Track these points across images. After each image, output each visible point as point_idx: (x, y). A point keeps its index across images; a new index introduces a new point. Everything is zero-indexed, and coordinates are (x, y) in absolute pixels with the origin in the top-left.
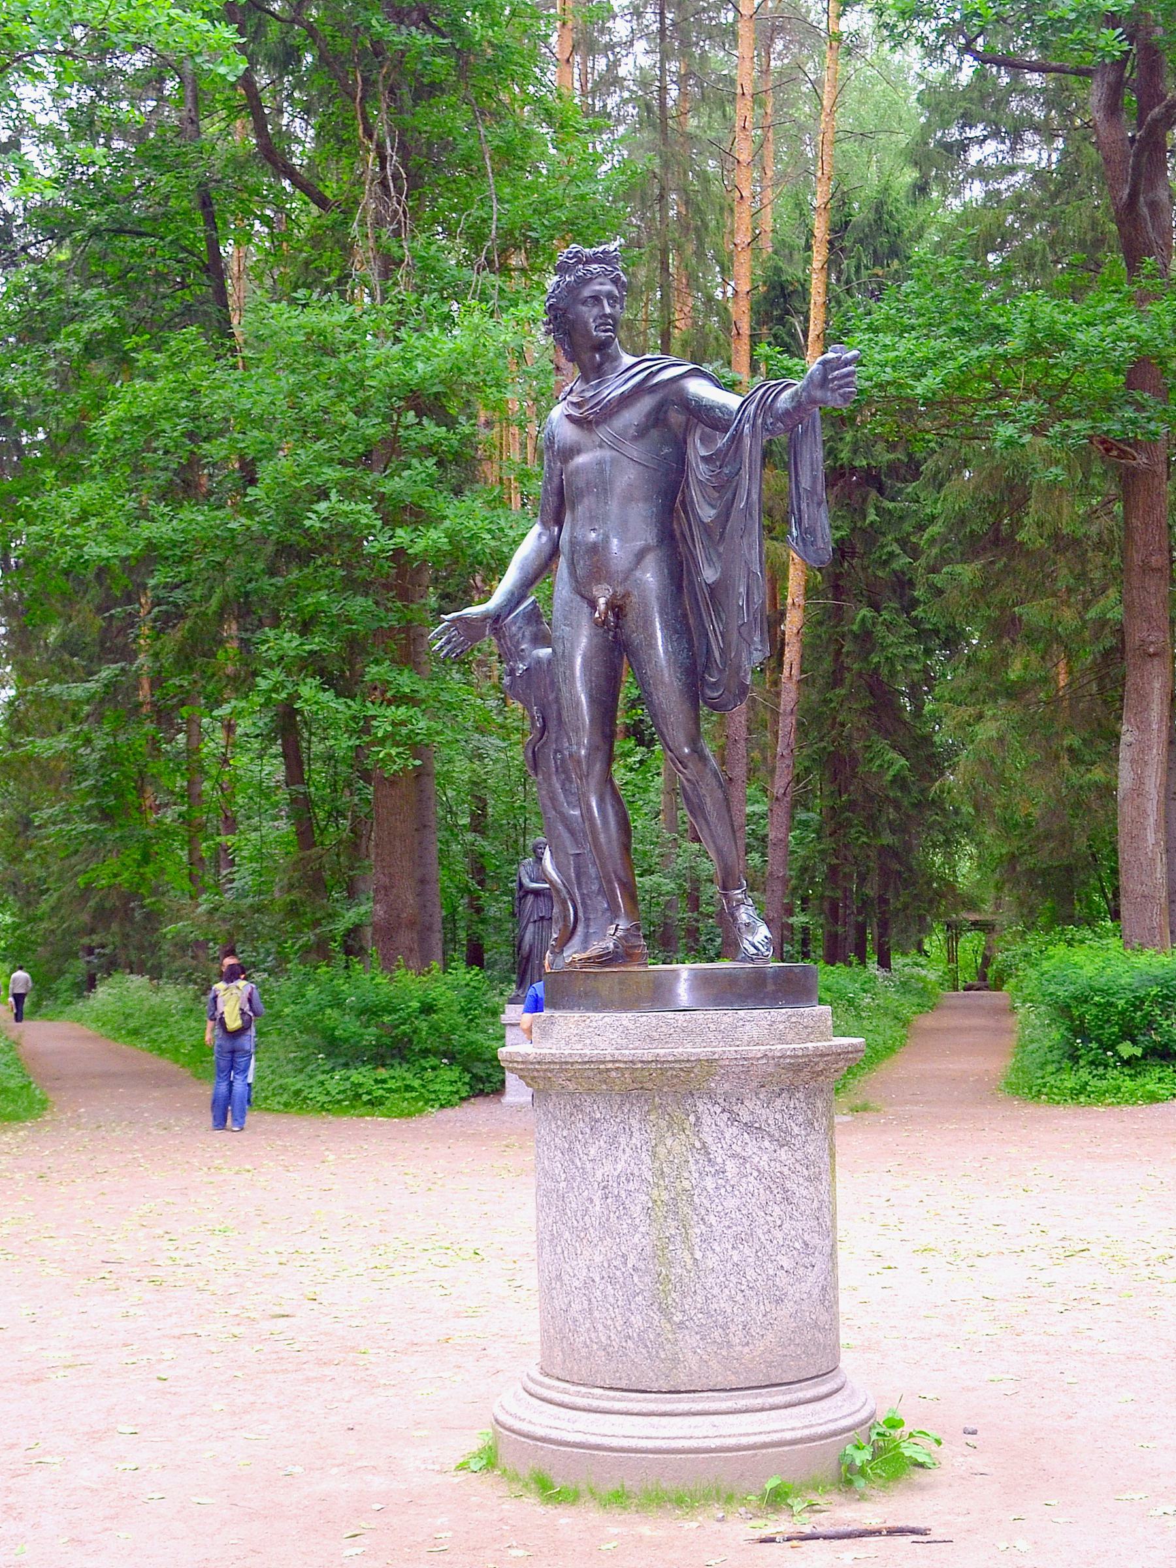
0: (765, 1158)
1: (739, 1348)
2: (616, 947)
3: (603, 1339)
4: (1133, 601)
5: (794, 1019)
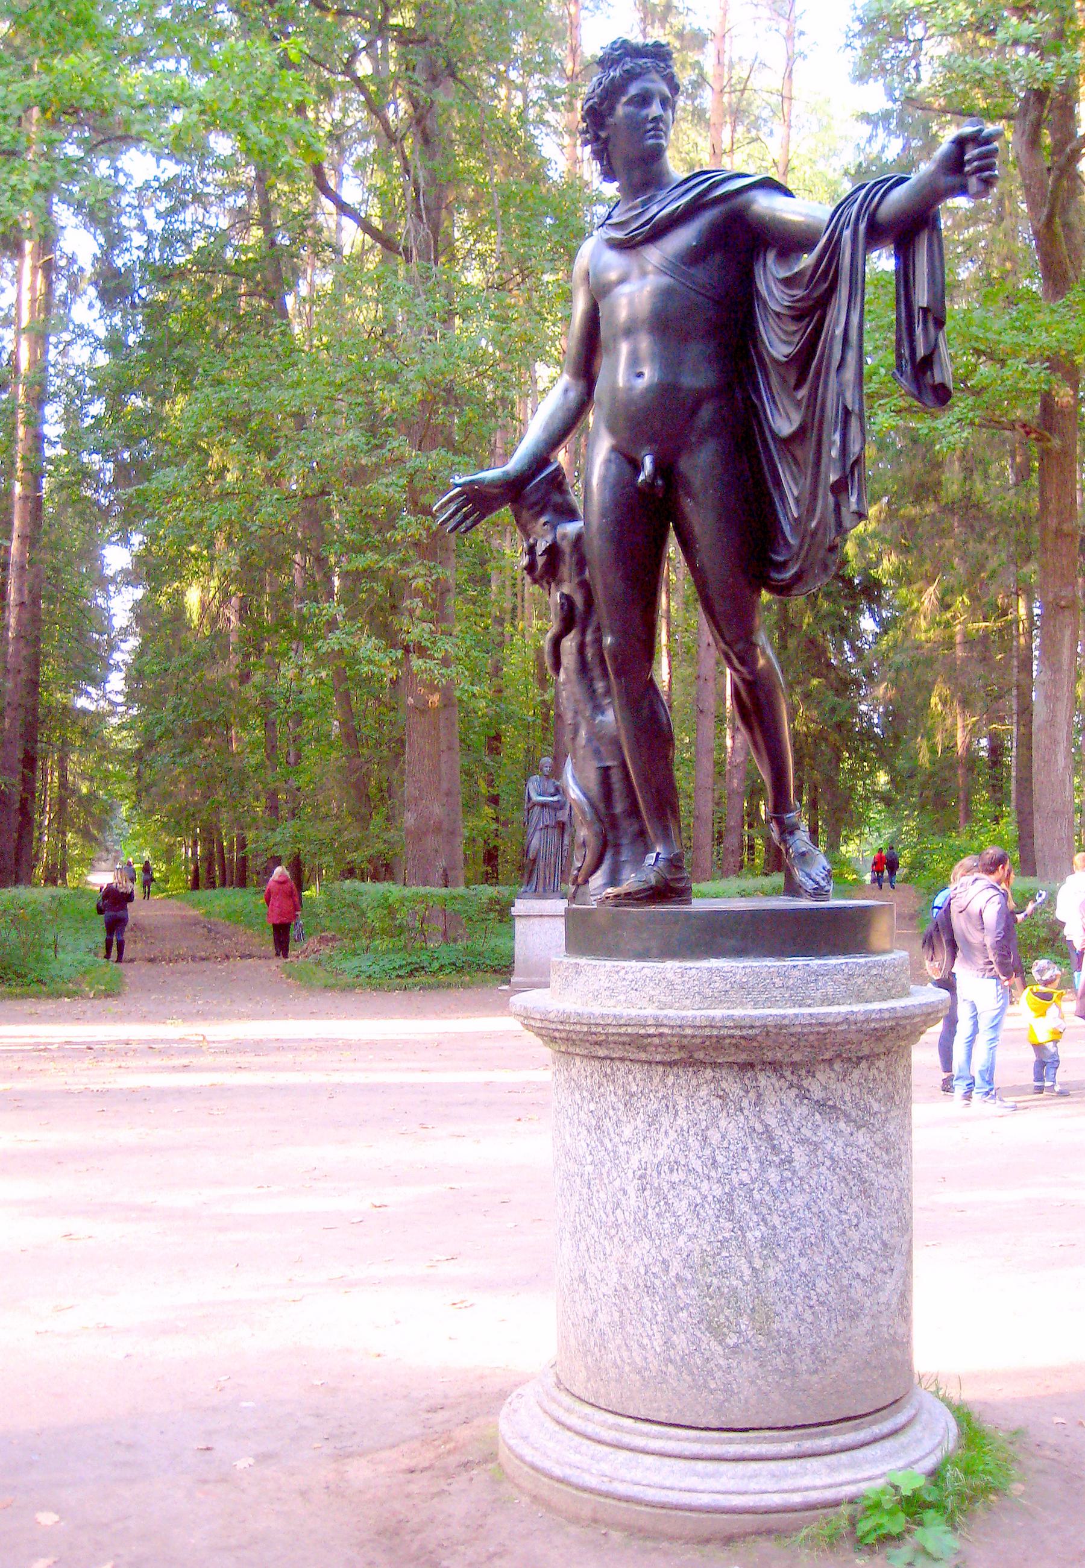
0: (840, 1142)
1: (805, 1376)
3: (638, 1360)
5: (874, 972)
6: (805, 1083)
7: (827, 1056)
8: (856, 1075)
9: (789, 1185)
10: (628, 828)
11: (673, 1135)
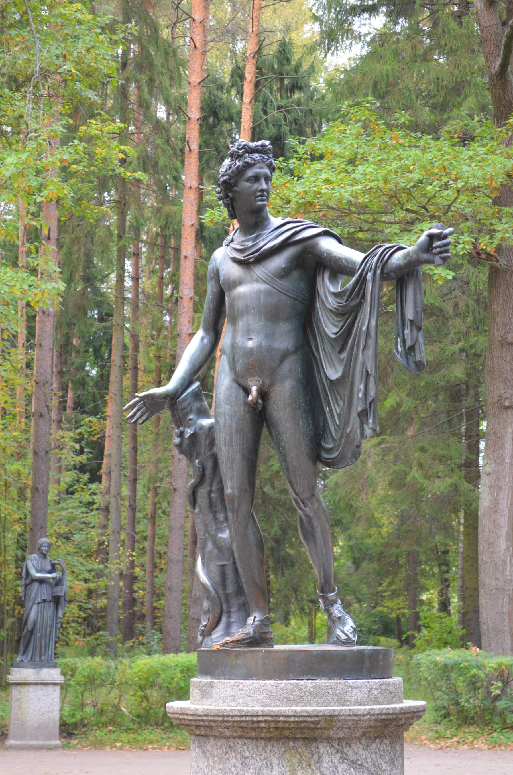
2: (255, 632)
4: (493, 367)
6: (345, 750)
8: (374, 746)
10: (235, 603)
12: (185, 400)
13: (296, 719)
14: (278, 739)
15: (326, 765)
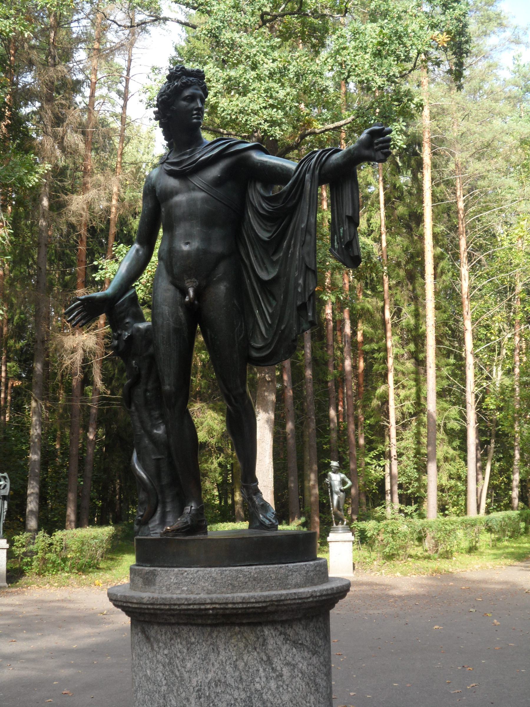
0: (305, 664)
2: (192, 521)
6: (288, 631)
7: (299, 616)
8: (312, 624)
9: (281, 689)
11: (217, 665)
12: (123, 304)
13: (245, 606)
14: (223, 624)
15: (270, 647)
